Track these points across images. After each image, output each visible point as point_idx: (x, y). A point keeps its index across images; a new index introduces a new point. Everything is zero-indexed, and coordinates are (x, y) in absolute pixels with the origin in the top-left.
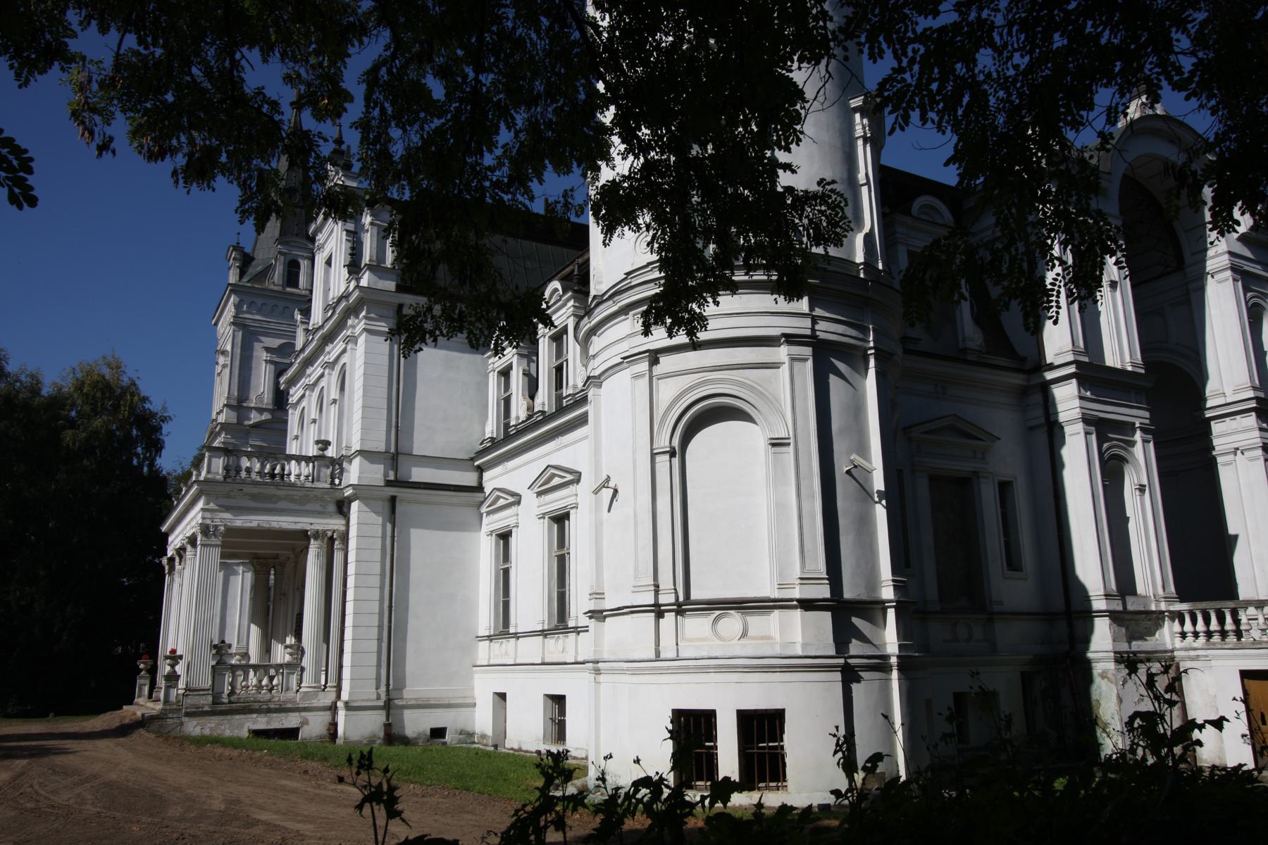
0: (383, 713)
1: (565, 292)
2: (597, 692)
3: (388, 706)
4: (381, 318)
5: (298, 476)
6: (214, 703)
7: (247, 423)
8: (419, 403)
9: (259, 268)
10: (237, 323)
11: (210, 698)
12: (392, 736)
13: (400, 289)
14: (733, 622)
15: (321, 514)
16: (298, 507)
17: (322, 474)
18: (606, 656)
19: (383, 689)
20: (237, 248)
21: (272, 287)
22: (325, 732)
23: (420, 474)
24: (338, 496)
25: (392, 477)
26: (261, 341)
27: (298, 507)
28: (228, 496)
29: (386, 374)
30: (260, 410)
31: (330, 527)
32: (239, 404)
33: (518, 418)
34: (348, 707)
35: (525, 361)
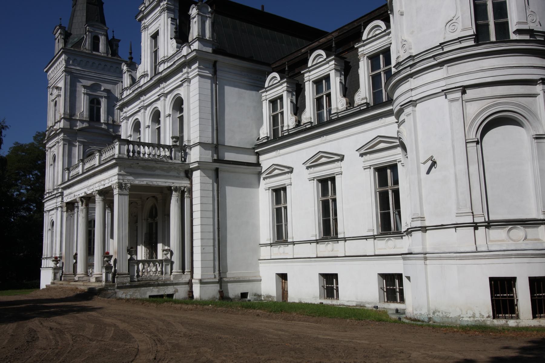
0: (218, 285)
1: (328, 56)
2: (426, 269)
3: (221, 282)
4: (206, 68)
5: (149, 155)
6: (131, 281)
7: (75, 128)
8: (227, 117)
9: (76, 40)
10: (67, 71)
11: (129, 279)
12: (223, 296)
13: (215, 52)
14: (519, 232)
15: (178, 178)
16: (166, 174)
17: (177, 156)
18: (428, 250)
19: (217, 272)
20: (61, 27)
21: (85, 51)
22: (187, 296)
23: (229, 156)
24: (186, 168)
25: (215, 158)
26: (80, 82)
27: (166, 174)
28: (130, 167)
29: (210, 100)
30: (82, 121)
31: (183, 185)
32: (70, 117)
33: (288, 126)
34: (201, 282)
35: (290, 95)
